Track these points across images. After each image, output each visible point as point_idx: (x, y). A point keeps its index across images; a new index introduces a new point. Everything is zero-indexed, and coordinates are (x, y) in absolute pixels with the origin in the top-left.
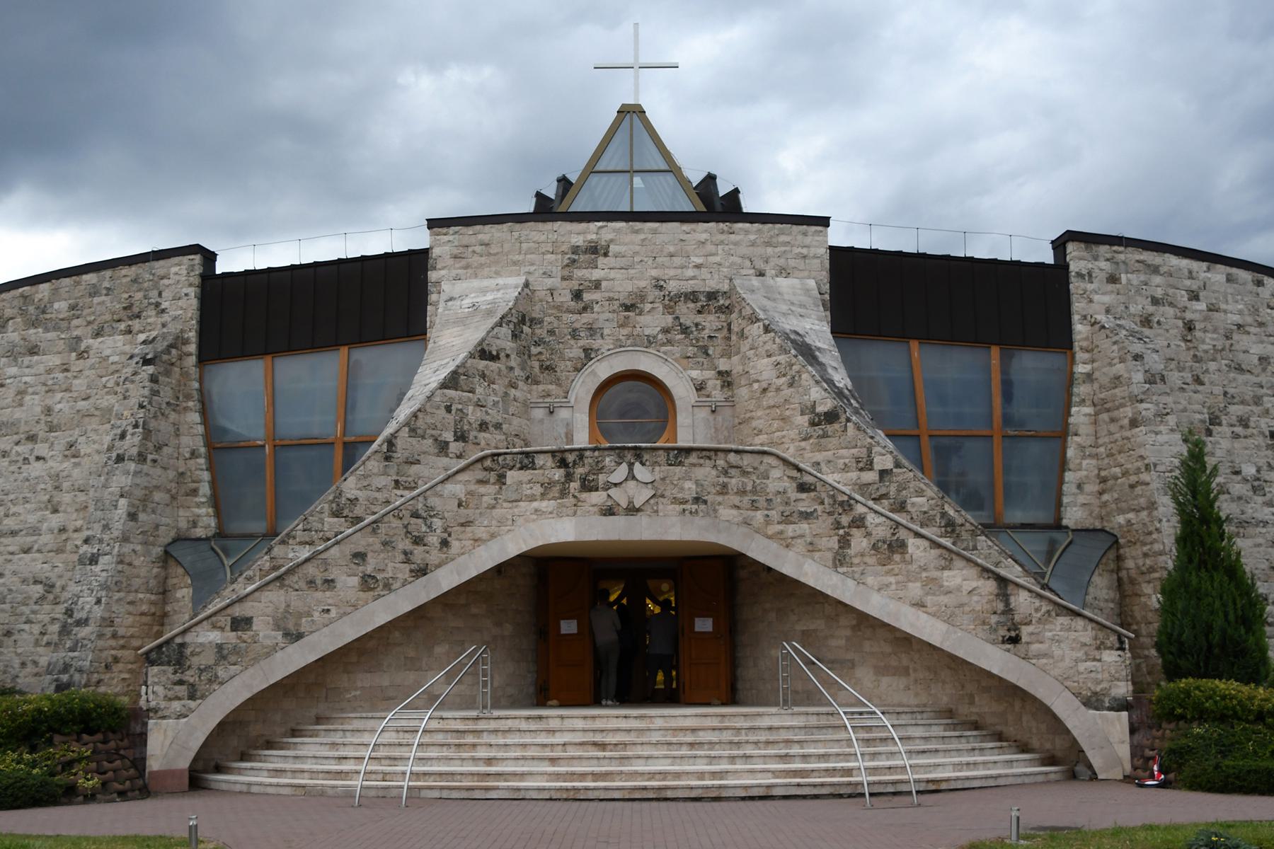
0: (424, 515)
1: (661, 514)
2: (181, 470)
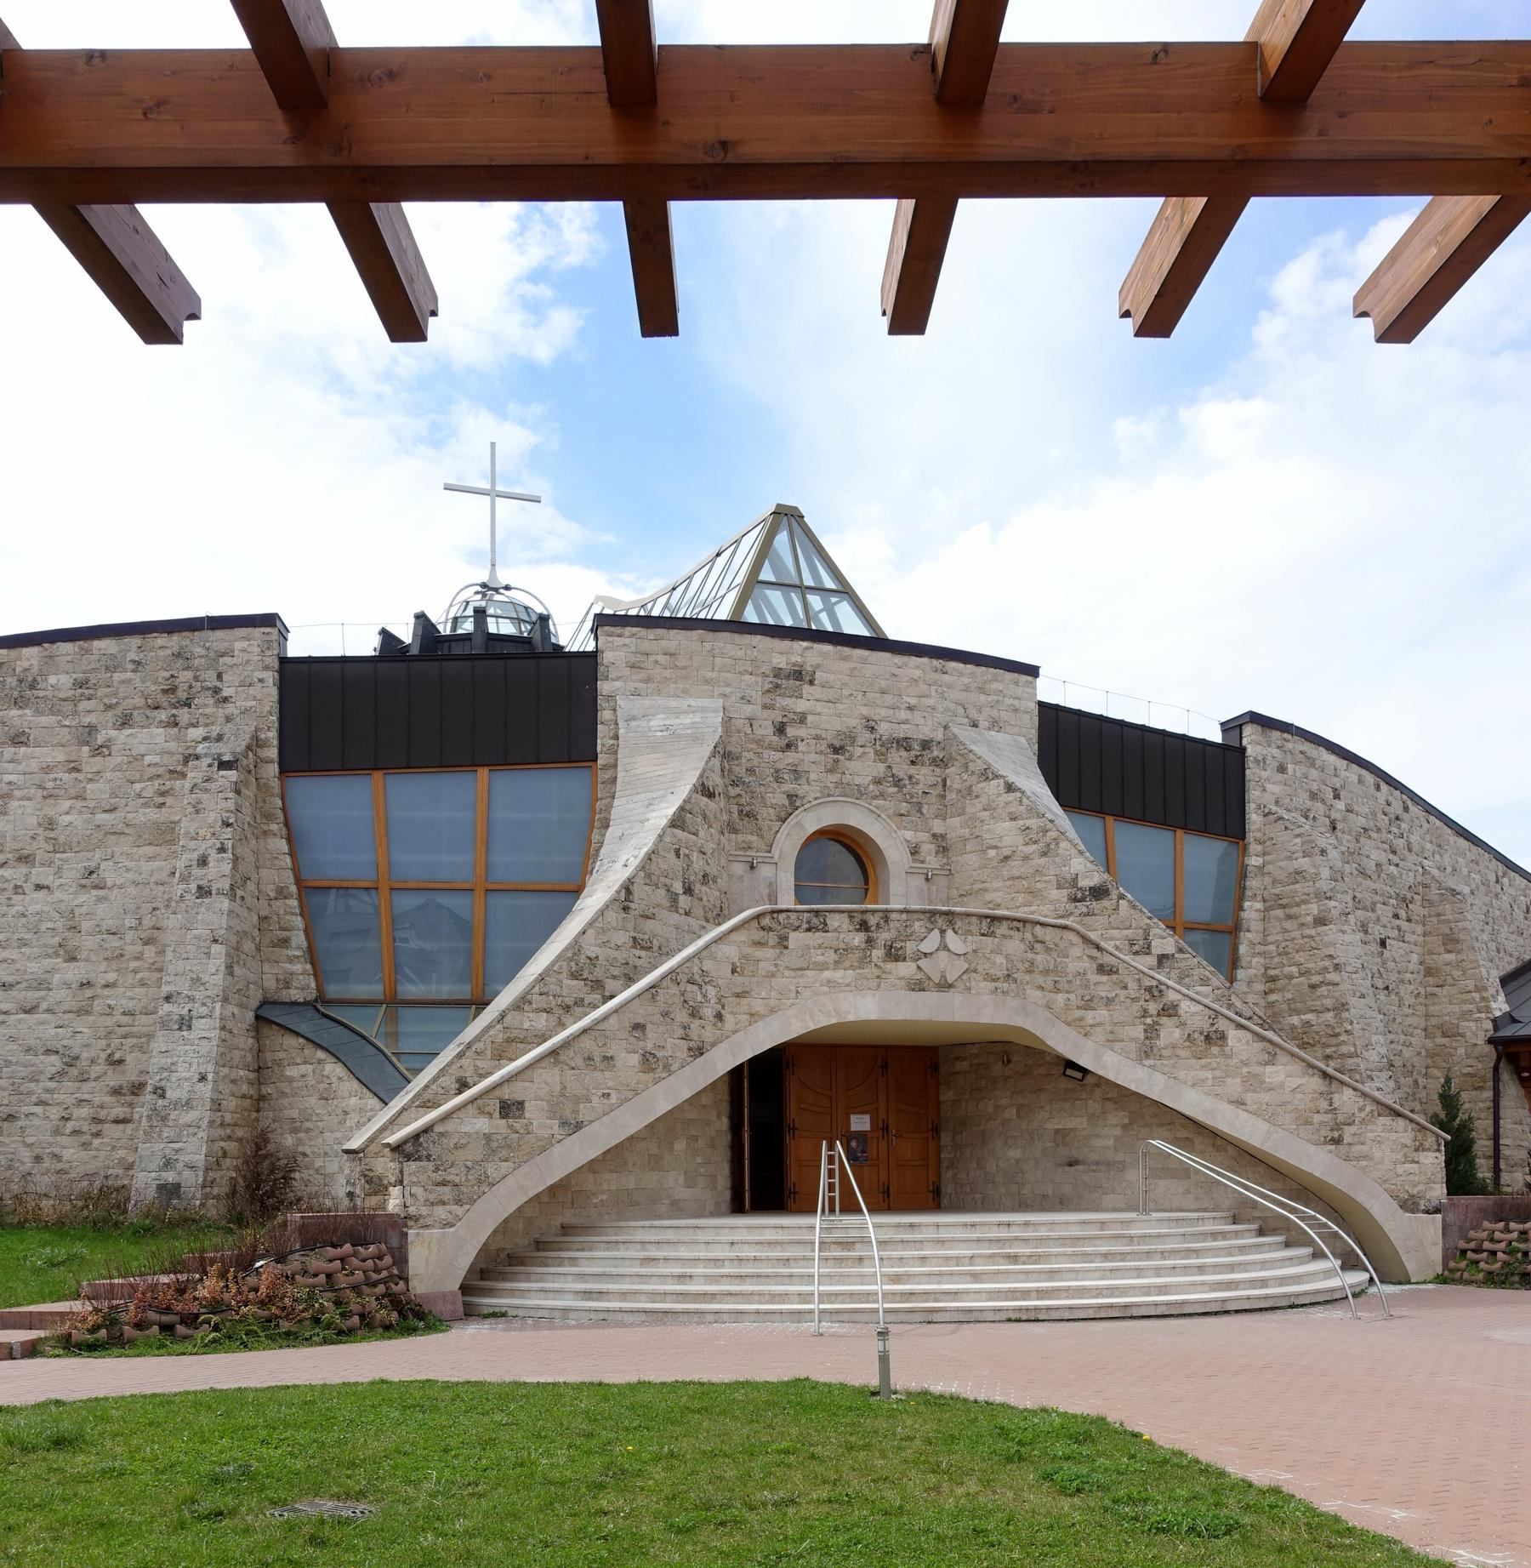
0: (699, 980)
1: (973, 991)
2: (263, 914)
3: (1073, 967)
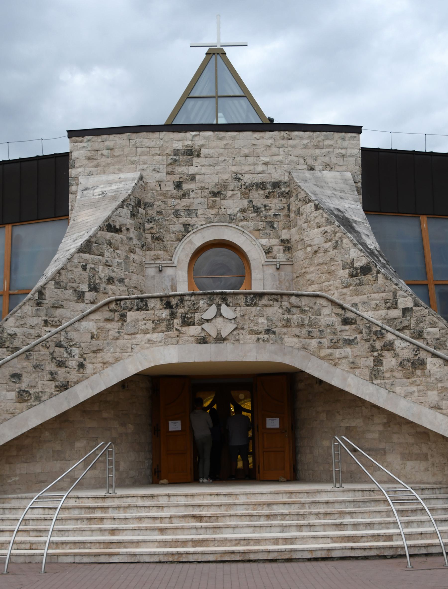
0: (65, 345)
1: (241, 342)
3: (324, 321)
